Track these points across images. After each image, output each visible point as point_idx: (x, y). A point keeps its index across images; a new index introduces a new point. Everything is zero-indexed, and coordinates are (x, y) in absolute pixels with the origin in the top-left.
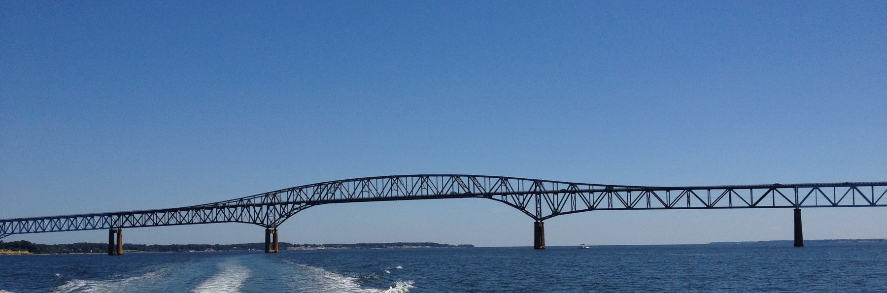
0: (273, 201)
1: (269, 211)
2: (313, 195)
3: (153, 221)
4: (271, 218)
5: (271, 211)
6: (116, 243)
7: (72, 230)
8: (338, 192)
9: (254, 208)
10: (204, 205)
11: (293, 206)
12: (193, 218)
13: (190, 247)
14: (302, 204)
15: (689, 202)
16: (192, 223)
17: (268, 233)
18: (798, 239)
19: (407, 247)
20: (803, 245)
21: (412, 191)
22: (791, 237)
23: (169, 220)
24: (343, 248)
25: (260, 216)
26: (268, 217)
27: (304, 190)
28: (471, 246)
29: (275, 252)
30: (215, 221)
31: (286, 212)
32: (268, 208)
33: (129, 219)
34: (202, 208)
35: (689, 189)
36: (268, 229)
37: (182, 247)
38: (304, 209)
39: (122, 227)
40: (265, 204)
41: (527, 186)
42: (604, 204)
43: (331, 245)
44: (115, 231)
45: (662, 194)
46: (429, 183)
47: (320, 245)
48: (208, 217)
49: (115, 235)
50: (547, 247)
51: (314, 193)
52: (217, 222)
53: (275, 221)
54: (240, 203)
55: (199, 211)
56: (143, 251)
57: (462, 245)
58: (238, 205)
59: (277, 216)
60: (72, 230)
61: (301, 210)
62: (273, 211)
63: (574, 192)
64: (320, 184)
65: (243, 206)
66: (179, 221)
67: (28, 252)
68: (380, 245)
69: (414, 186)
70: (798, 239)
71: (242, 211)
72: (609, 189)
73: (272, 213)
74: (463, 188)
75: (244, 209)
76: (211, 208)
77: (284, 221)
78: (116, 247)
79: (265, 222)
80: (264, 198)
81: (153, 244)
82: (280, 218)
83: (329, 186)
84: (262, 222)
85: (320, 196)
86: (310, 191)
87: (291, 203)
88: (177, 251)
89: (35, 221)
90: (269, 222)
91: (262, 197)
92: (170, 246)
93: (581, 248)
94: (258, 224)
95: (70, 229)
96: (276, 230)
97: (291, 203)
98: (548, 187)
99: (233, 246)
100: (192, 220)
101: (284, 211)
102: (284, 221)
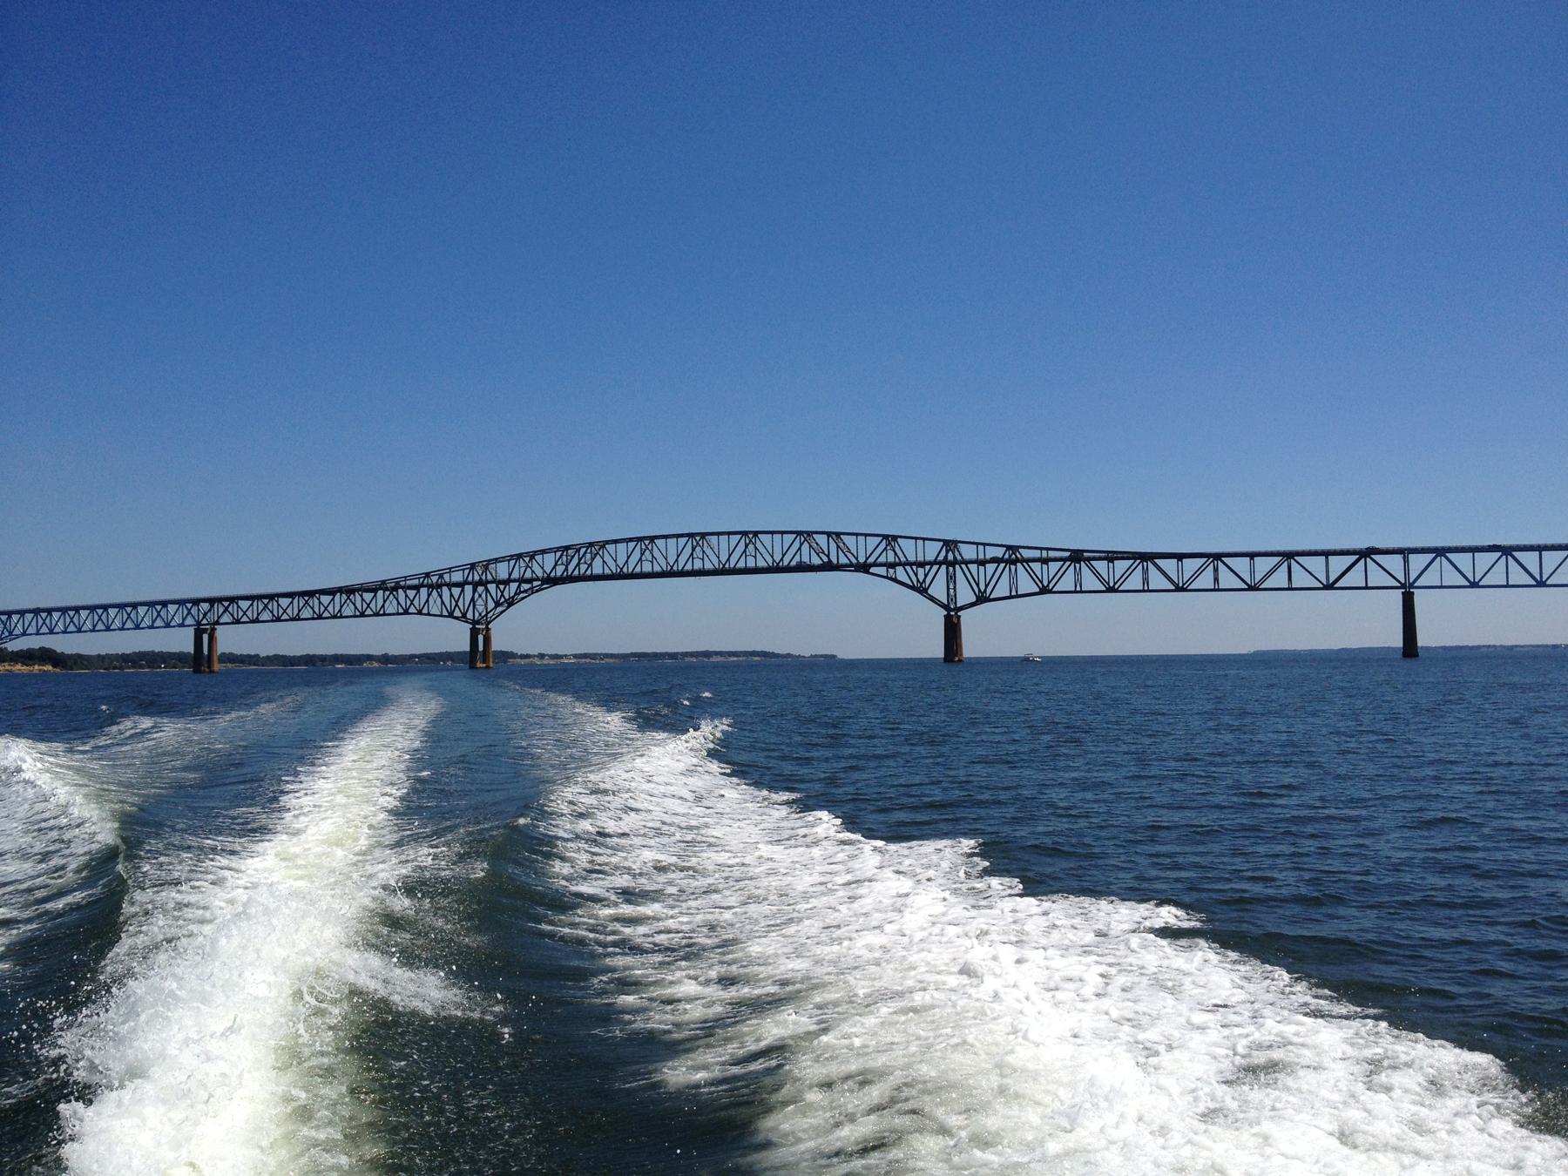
0: (484, 577)
1: (476, 595)
2: (554, 567)
3: (272, 612)
4: (481, 608)
5: (480, 596)
6: (206, 651)
7: (43, 634)
8: (598, 562)
9: (450, 590)
11: (519, 587)
12: (341, 607)
13: (337, 658)
14: (535, 583)
15: (1216, 579)
16: (341, 617)
17: (474, 634)
18: (1410, 646)
19: (719, 659)
20: (1417, 656)
21: (728, 559)
22: (1397, 641)
23: (299, 611)
24: (607, 660)
25: (460, 604)
26: (474, 606)
28: (833, 657)
29: (488, 667)
30: (382, 612)
32: (475, 591)
33: (230, 609)
34: (358, 590)
35: (1218, 557)
36: (949, 614)
37: (323, 659)
38: (537, 591)
39: (217, 623)
40: (469, 584)
41: (932, 551)
42: (1067, 582)
43: (585, 656)
44: (205, 631)
45: (1169, 565)
46: (759, 545)
47: (566, 656)
48: (368, 605)
49: (205, 637)
50: (1427, 649)
51: (556, 564)
53: (487, 613)
56: (255, 665)
57: (816, 656)
58: (466, 583)
59: (491, 605)
60: (43, 634)
61: (533, 593)
62: (484, 596)
63: (1014, 562)
64: (567, 548)
65: (431, 587)
67: (50, 668)
68: (673, 656)
70: (1410, 646)
71: (429, 595)
72: (1077, 557)
76: (374, 590)
77: (502, 612)
78: (206, 658)
79: (469, 615)
80: (467, 572)
81: (271, 653)
82: (495, 608)
83: (583, 550)
84: (464, 615)
85: (566, 569)
86: (549, 560)
87: (515, 581)
88: (314, 665)
89: (63, 614)
90: (477, 615)
91: (463, 570)
92: (301, 657)
93: (1026, 660)
94: (457, 618)
96: (488, 629)
97: (515, 581)
98: (968, 552)
99: (413, 657)
100: (340, 611)
101: (502, 595)
102: (502, 612)
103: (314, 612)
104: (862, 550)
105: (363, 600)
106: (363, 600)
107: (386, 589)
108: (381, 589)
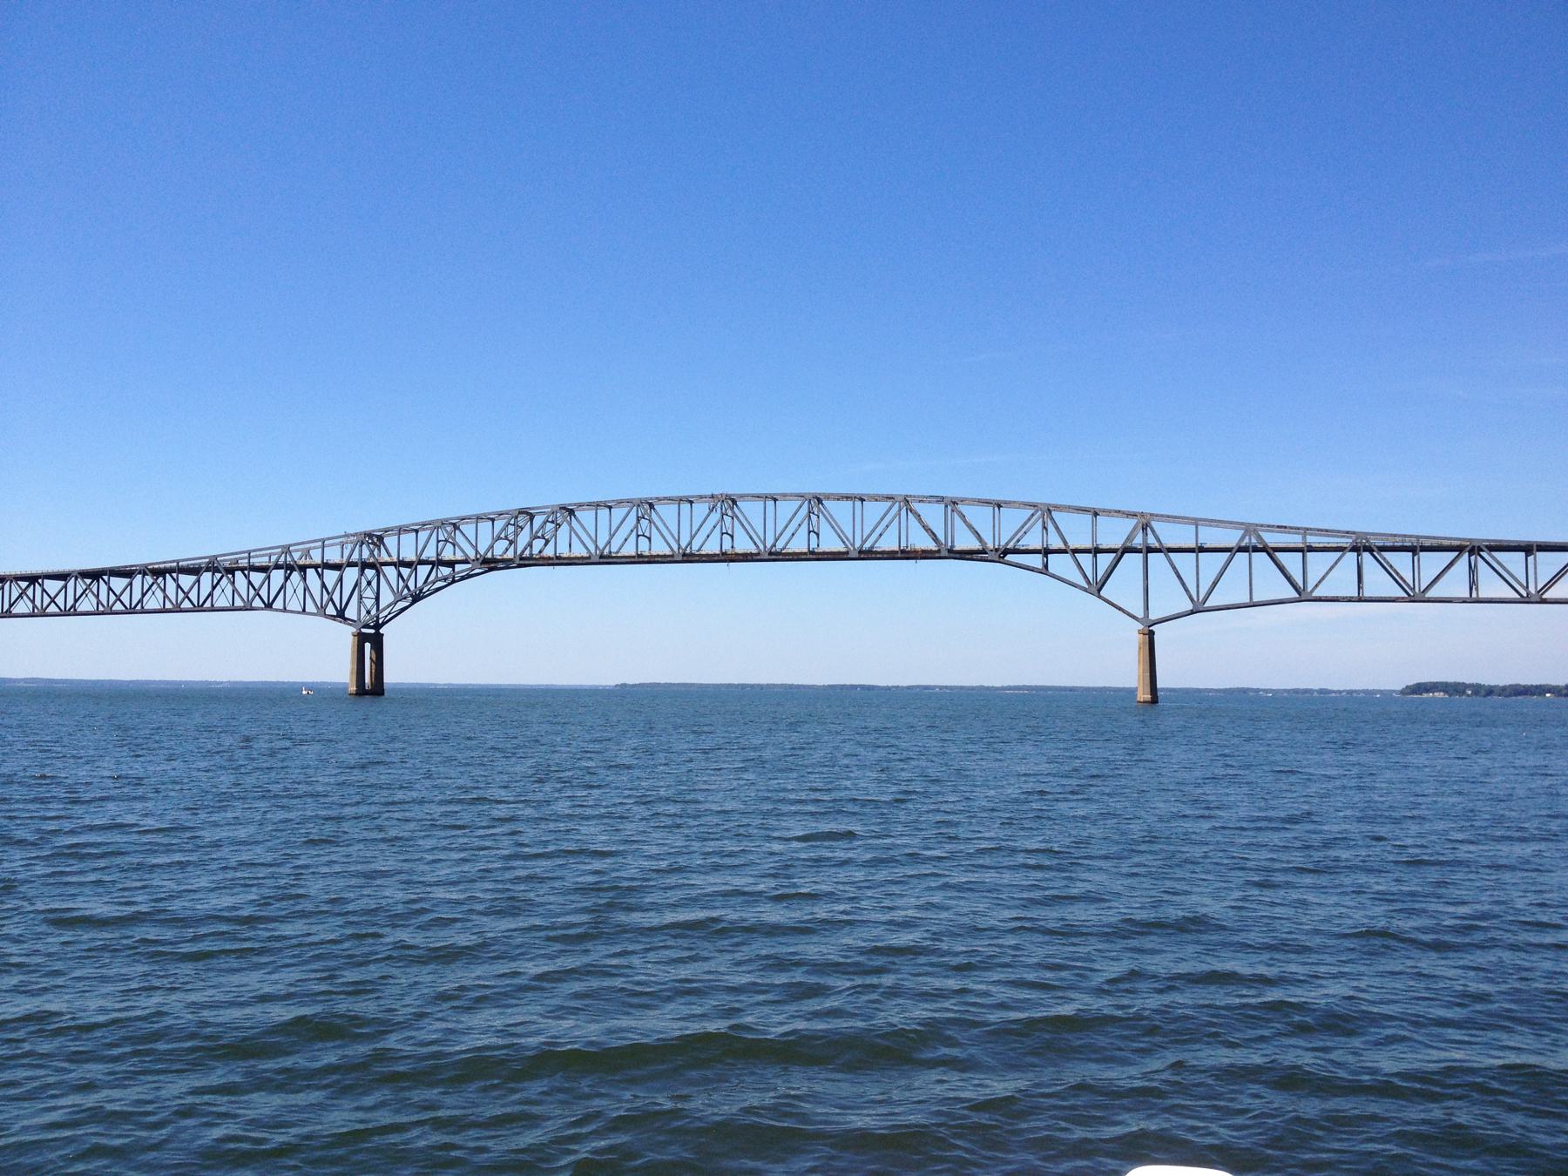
2: (492, 547)
5: (369, 583)
10: (178, 562)
12: (144, 595)
15: (1473, 584)
16: (77, 614)
21: (609, 542)
23: (76, 601)
27: (469, 529)
30: (208, 604)
31: (412, 587)
33: (30, 592)
35: (1474, 549)
38: (463, 578)
41: (1113, 533)
45: (1513, 562)
52: (213, 609)
54: (282, 559)
55: (161, 579)
62: (374, 584)
65: (289, 568)
66: (39, 607)
69: (696, 533)
70: (371, 687)
71: (287, 578)
73: (372, 589)
74: (810, 532)
75: (290, 574)
76: (195, 571)
79: (351, 613)
90: (363, 612)
95: (15, 610)
100: (141, 601)
103: (35, 606)
104: (483, 539)
105: (178, 586)
106: (178, 586)
107: (215, 570)
108: (207, 570)
